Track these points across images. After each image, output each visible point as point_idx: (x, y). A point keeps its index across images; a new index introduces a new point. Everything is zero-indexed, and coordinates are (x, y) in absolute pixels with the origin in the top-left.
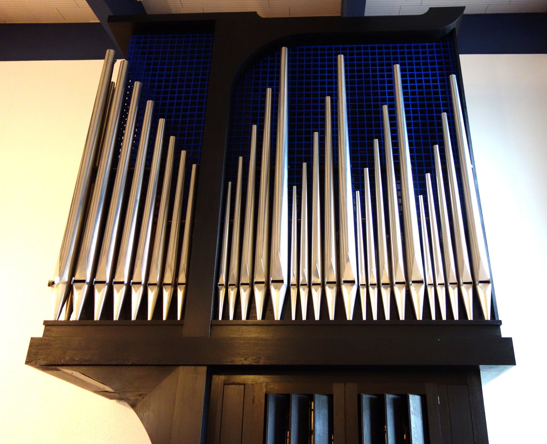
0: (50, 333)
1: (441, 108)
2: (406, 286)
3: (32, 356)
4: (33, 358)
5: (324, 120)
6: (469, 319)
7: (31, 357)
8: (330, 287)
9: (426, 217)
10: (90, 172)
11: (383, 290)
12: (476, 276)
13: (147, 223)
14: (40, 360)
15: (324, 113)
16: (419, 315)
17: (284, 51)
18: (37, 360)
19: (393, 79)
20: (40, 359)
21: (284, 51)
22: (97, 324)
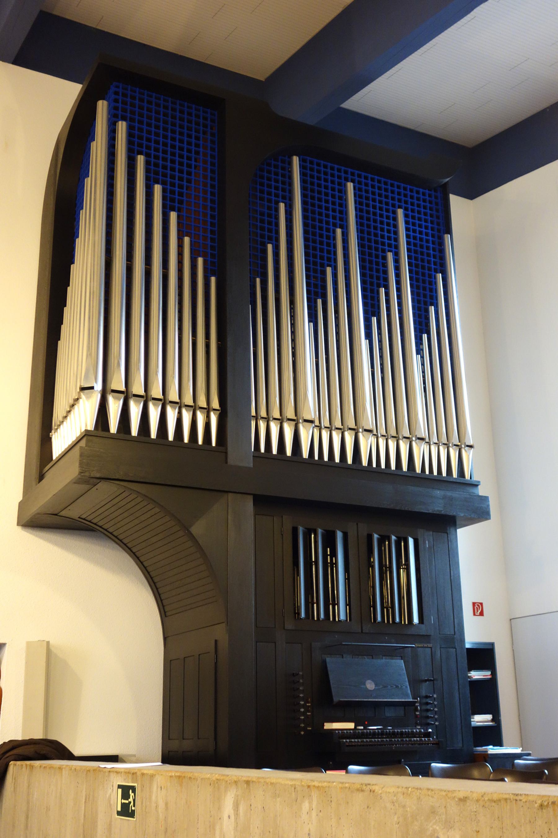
0: (93, 444)
1: (373, 266)
2: (193, 409)
3: (85, 467)
4: (86, 468)
5: (277, 232)
6: (304, 457)
7: (83, 467)
8: (154, 404)
9: (316, 358)
10: (113, 249)
11: (169, 409)
12: (108, 382)
13: (157, 329)
14: (94, 472)
15: (277, 225)
16: (305, 454)
17: (296, 160)
18: (91, 472)
19: (394, 257)
20: (93, 471)
21: (296, 160)
22: (113, 437)
